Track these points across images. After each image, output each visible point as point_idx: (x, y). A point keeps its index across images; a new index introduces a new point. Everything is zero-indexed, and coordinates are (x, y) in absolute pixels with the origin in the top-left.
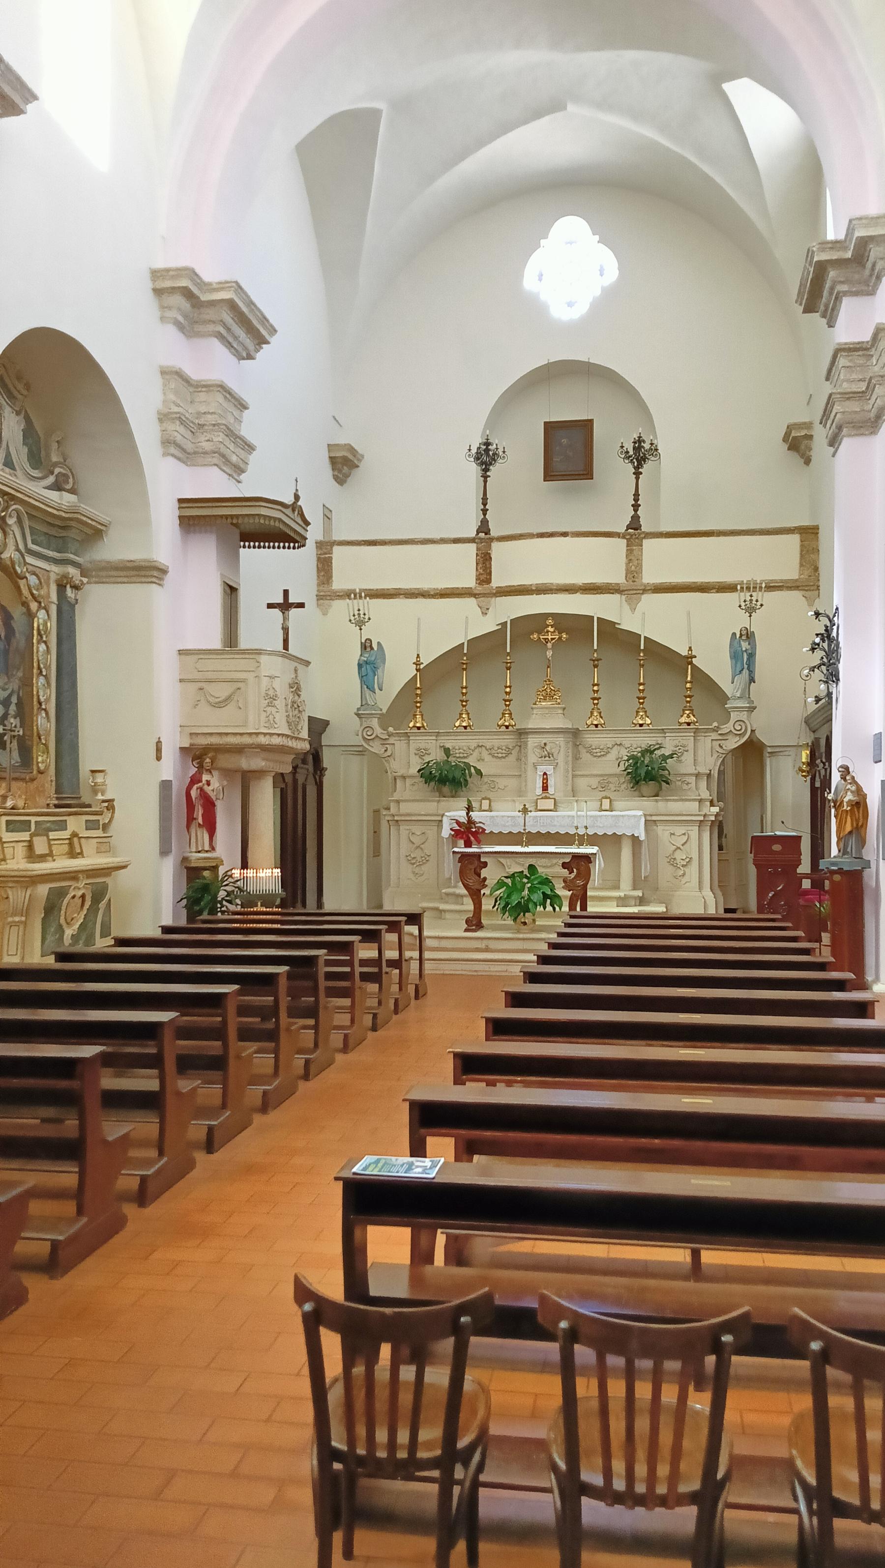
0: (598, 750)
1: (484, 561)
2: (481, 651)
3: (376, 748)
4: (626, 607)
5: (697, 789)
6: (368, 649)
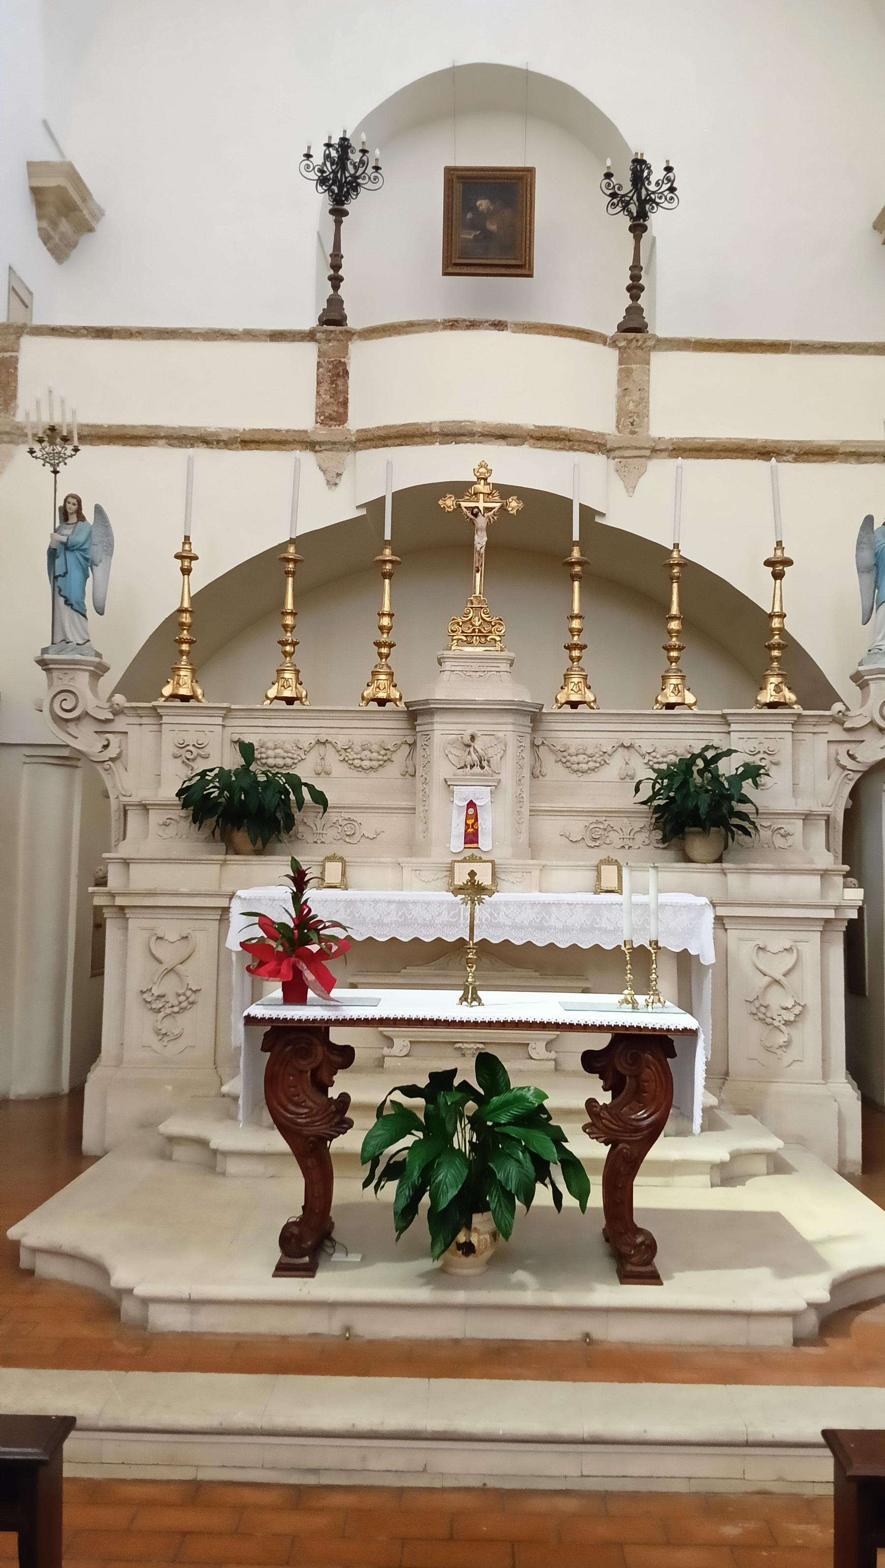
0: (581, 758)
1: (334, 377)
2: (325, 570)
3: (85, 740)
4: (617, 484)
5: (806, 846)
6: (73, 519)
